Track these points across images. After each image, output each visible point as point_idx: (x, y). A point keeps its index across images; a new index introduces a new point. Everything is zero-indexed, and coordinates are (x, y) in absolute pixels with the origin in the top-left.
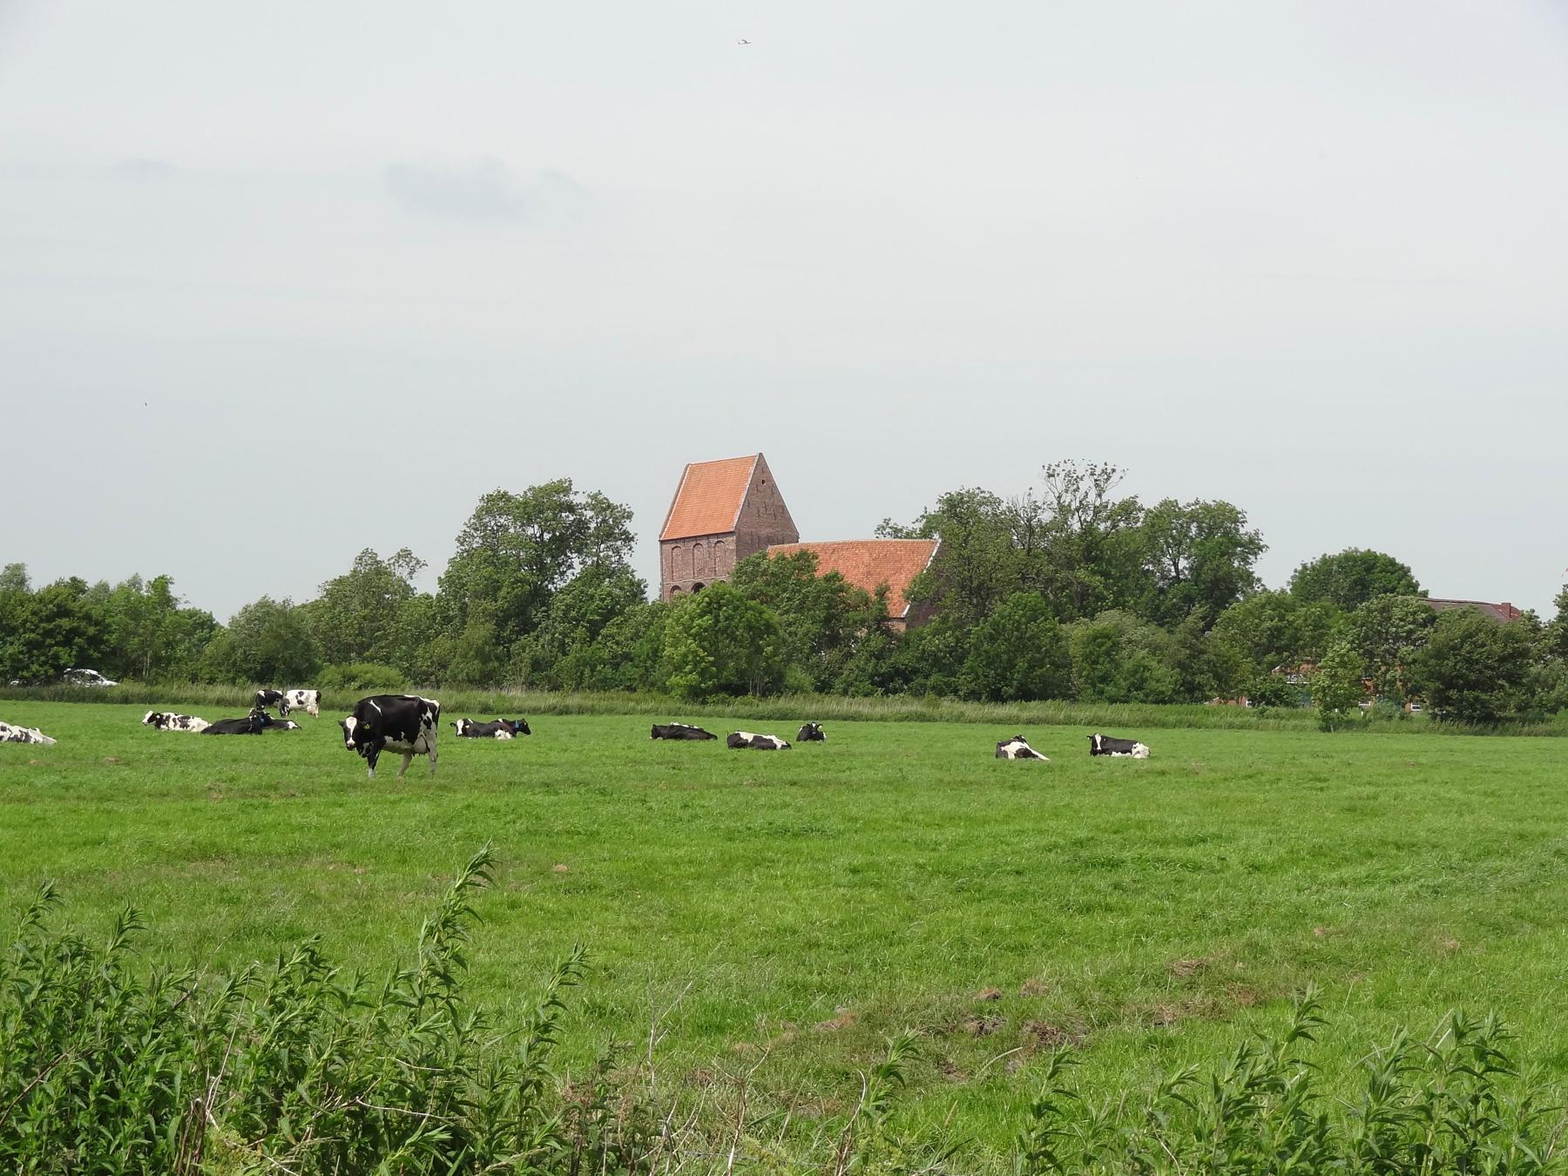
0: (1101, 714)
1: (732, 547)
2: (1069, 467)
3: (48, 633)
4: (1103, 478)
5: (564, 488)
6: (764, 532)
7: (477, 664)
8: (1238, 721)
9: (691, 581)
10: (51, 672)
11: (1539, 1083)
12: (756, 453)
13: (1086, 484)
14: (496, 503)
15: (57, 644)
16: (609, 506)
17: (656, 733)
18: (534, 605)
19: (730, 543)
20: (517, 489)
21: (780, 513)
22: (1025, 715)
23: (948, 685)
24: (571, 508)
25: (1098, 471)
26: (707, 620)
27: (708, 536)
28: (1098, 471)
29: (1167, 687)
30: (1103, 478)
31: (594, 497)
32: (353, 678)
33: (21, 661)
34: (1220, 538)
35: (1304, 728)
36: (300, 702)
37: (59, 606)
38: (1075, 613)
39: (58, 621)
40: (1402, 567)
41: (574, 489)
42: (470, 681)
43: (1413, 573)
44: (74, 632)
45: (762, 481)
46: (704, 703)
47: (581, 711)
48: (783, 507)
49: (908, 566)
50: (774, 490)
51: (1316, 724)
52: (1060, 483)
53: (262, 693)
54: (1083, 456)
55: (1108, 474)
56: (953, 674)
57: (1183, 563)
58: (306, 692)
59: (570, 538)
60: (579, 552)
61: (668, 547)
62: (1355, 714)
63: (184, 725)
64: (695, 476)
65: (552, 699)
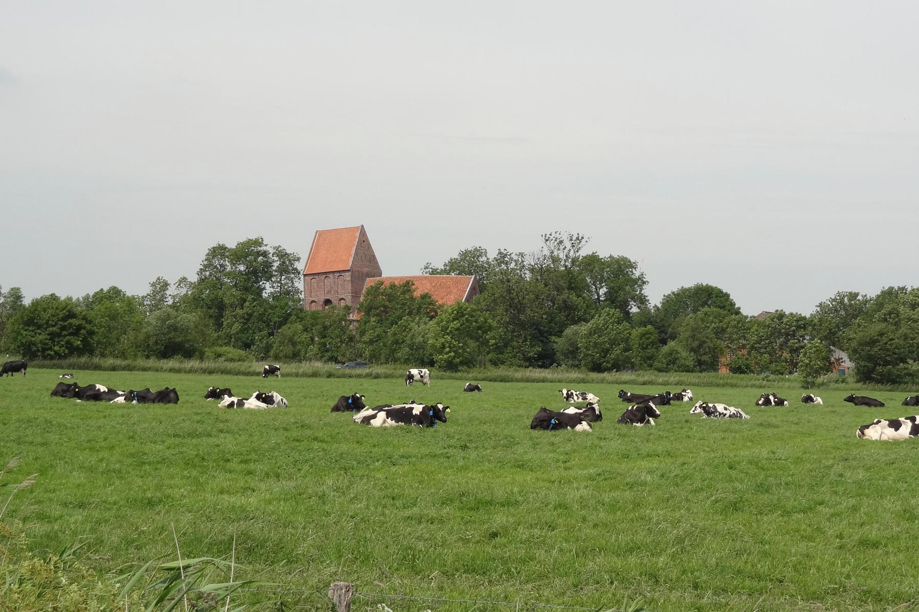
0: (682, 379)
1: (349, 278)
2: (557, 235)
3: (63, 328)
4: (577, 241)
5: (258, 242)
6: (365, 270)
7: (290, 347)
8: (750, 383)
9: (322, 298)
10: (67, 351)
11: (341, 556)
12: (359, 225)
13: (568, 244)
14: (218, 251)
15: (70, 334)
16: (286, 254)
17: (851, 399)
18: (242, 310)
19: (347, 276)
20: (232, 244)
21: (372, 259)
22: (641, 379)
23: (499, 359)
24: (265, 254)
25: (574, 238)
26: (456, 324)
27: (333, 272)
28: (574, 238)
29: (690, 363)
30: (577, 241)
31: (277, 248)
32: (220, 355)
33: (47, 344)
34: (620, 277)
35: (794, 388)
36: (422, 377)
37: (69, 311)
38: (553, 319)
39: (70, 321)
40: (884, 293)
41: (265, 243)
42: (286, 357)
43: (731, 297)
44: (79, 328)
45: (363, 242)
46: (457, 371)
47: (387, 376)
48: (374, 256)
49: (455, 291)
50: (369, 247)
51: (800, 385)
52: (552, 245)
53: (267, 367)
54: (566, 228)
55: (579, 239)
56: (502, 353)
57: (603, 291)
58: (424, 370)
59: (265, 272)
60: (523, 279)
61: (308, 278)
62: (820, 380)
63: (584, 399)
64: (322, 237)
65: (332, 367)
